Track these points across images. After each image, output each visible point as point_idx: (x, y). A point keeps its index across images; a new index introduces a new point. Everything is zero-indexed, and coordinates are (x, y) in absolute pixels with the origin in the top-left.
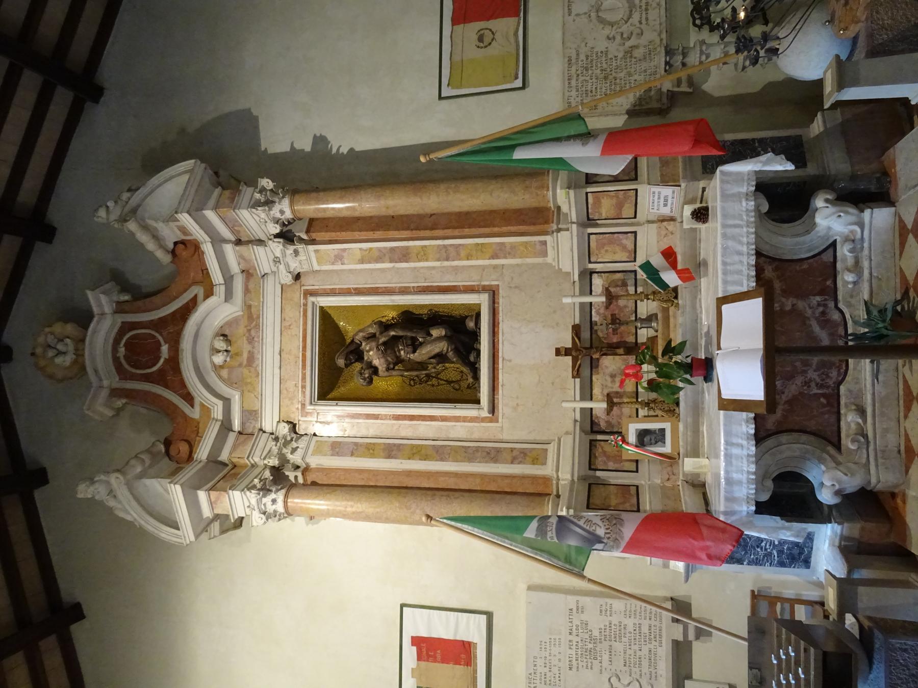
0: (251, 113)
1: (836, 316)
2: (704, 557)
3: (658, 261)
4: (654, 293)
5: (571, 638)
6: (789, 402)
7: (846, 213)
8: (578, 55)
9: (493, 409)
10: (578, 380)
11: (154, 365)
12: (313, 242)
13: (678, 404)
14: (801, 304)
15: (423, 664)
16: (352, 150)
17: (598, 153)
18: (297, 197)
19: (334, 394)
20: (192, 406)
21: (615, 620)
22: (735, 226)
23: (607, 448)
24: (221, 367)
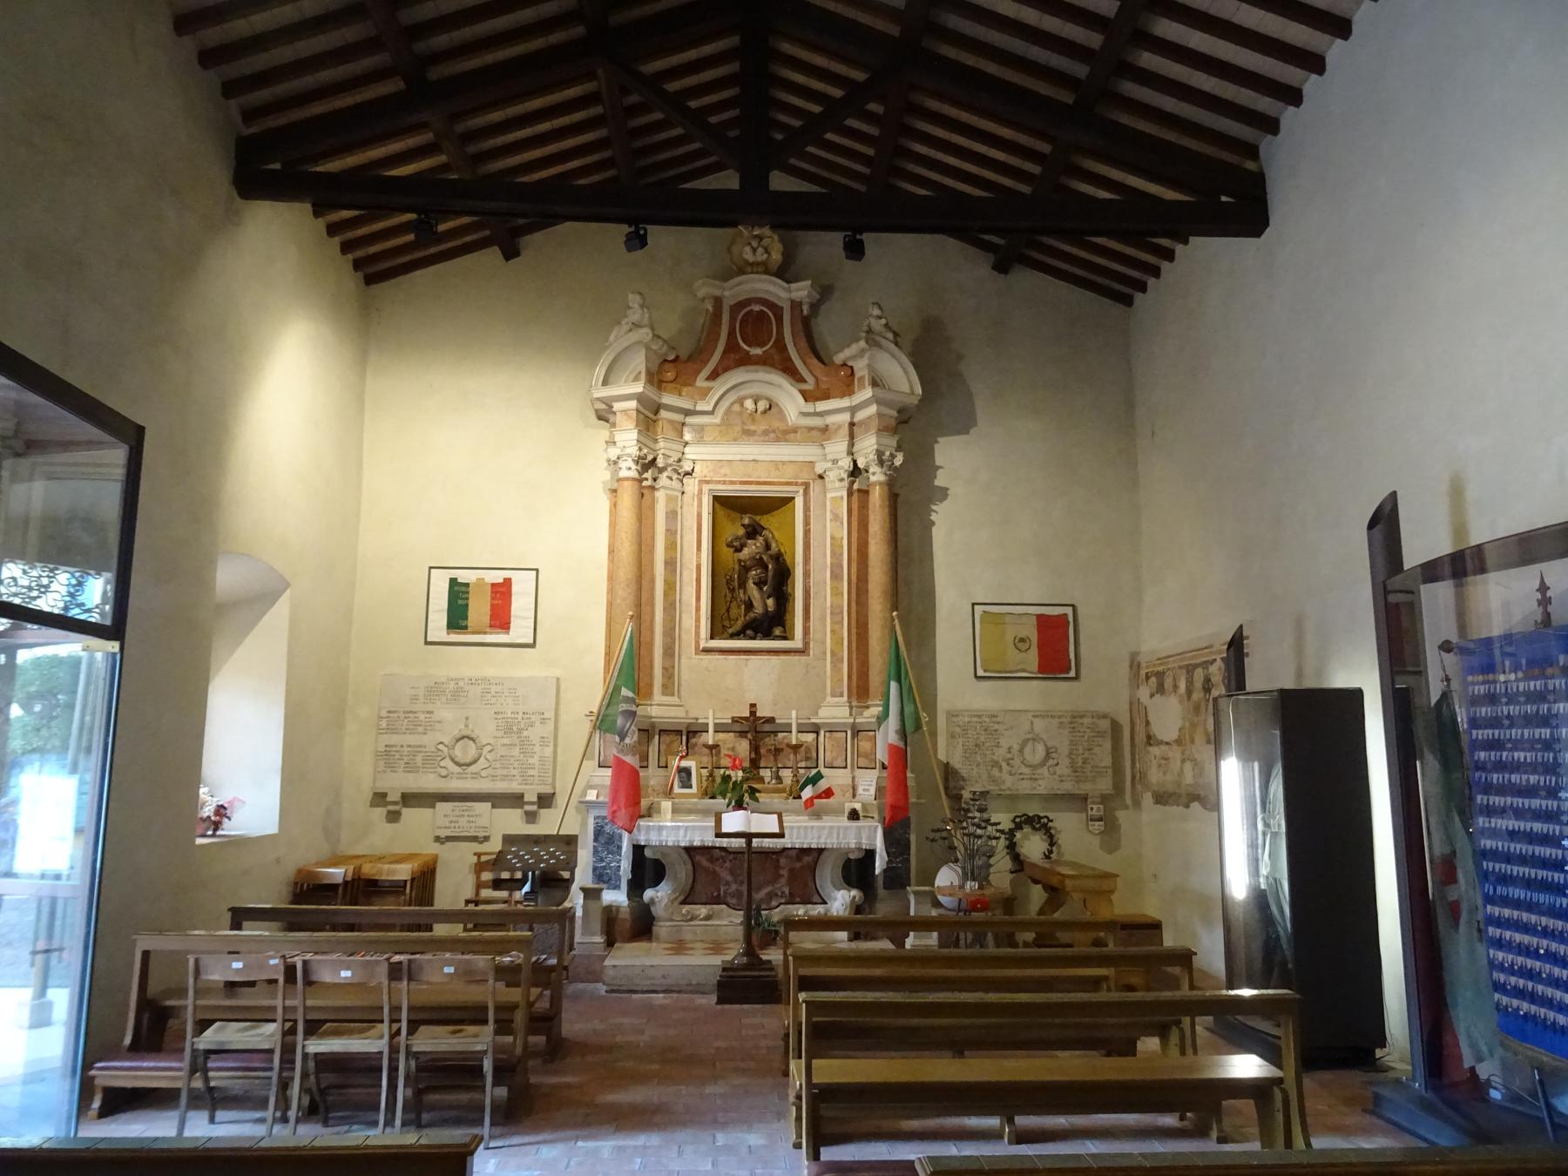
0: (971, 427)
1: (774, 903)
2: (615, 808)
3: (823, 785)
4: (798, 781)
5: (521, 714)
6: (715, 872)
7: (846, 909)
8: (998, 723)
9: (707, 651)
10: (730, 721)
11: (744, 342)
12: (850, 493)
13: (713, 797)
14: (783, 881)
15: (489, 588)
16: (933, 523)
17: (890, 742)
18: (886, 488)
19: (717, 505)
20: (708, 379)
21: (537, 749)
22: (838, 835)
23: (677, 743)
24: (742, 405)
